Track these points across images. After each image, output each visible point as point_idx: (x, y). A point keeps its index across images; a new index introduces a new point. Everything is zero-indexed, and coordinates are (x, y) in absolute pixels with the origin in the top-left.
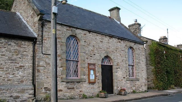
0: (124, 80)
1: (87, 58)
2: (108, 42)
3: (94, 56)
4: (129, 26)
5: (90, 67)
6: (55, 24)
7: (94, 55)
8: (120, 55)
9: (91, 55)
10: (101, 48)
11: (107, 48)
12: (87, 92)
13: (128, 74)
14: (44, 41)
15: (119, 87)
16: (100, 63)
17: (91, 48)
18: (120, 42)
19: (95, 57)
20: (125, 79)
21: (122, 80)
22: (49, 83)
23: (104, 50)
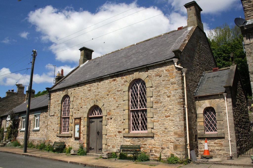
0: (119, 136)
1: (75, 113)
2: (97, 88)
3: (81, 109)
4: (137, 44)
5: (76, 122)
6: (200, 27)
7: (81, 107)
8: (115, 98)
9: (79, 109)
10: (89, 98)
11: (96, 96)
12: (197, 90)
13: (127, 126)
14: (51, 106)
15: (109, 146)
16: (86, 115)
17: (79, 101)
18: (114, 80)
19: (81, 110)
20: (122, 135)
21: (116, 136)
22: (51, 137)
23: (92, 99)
